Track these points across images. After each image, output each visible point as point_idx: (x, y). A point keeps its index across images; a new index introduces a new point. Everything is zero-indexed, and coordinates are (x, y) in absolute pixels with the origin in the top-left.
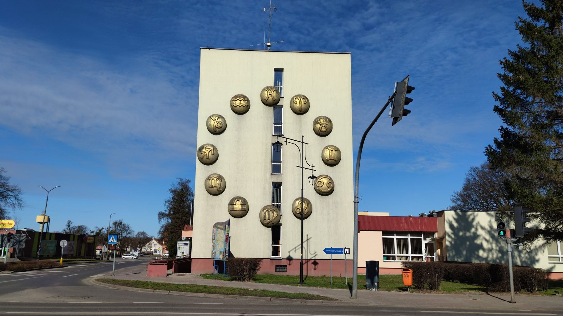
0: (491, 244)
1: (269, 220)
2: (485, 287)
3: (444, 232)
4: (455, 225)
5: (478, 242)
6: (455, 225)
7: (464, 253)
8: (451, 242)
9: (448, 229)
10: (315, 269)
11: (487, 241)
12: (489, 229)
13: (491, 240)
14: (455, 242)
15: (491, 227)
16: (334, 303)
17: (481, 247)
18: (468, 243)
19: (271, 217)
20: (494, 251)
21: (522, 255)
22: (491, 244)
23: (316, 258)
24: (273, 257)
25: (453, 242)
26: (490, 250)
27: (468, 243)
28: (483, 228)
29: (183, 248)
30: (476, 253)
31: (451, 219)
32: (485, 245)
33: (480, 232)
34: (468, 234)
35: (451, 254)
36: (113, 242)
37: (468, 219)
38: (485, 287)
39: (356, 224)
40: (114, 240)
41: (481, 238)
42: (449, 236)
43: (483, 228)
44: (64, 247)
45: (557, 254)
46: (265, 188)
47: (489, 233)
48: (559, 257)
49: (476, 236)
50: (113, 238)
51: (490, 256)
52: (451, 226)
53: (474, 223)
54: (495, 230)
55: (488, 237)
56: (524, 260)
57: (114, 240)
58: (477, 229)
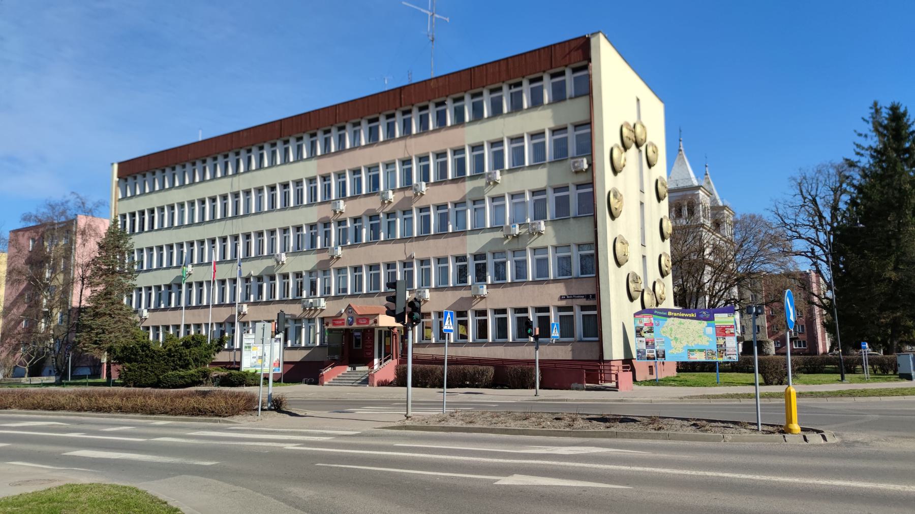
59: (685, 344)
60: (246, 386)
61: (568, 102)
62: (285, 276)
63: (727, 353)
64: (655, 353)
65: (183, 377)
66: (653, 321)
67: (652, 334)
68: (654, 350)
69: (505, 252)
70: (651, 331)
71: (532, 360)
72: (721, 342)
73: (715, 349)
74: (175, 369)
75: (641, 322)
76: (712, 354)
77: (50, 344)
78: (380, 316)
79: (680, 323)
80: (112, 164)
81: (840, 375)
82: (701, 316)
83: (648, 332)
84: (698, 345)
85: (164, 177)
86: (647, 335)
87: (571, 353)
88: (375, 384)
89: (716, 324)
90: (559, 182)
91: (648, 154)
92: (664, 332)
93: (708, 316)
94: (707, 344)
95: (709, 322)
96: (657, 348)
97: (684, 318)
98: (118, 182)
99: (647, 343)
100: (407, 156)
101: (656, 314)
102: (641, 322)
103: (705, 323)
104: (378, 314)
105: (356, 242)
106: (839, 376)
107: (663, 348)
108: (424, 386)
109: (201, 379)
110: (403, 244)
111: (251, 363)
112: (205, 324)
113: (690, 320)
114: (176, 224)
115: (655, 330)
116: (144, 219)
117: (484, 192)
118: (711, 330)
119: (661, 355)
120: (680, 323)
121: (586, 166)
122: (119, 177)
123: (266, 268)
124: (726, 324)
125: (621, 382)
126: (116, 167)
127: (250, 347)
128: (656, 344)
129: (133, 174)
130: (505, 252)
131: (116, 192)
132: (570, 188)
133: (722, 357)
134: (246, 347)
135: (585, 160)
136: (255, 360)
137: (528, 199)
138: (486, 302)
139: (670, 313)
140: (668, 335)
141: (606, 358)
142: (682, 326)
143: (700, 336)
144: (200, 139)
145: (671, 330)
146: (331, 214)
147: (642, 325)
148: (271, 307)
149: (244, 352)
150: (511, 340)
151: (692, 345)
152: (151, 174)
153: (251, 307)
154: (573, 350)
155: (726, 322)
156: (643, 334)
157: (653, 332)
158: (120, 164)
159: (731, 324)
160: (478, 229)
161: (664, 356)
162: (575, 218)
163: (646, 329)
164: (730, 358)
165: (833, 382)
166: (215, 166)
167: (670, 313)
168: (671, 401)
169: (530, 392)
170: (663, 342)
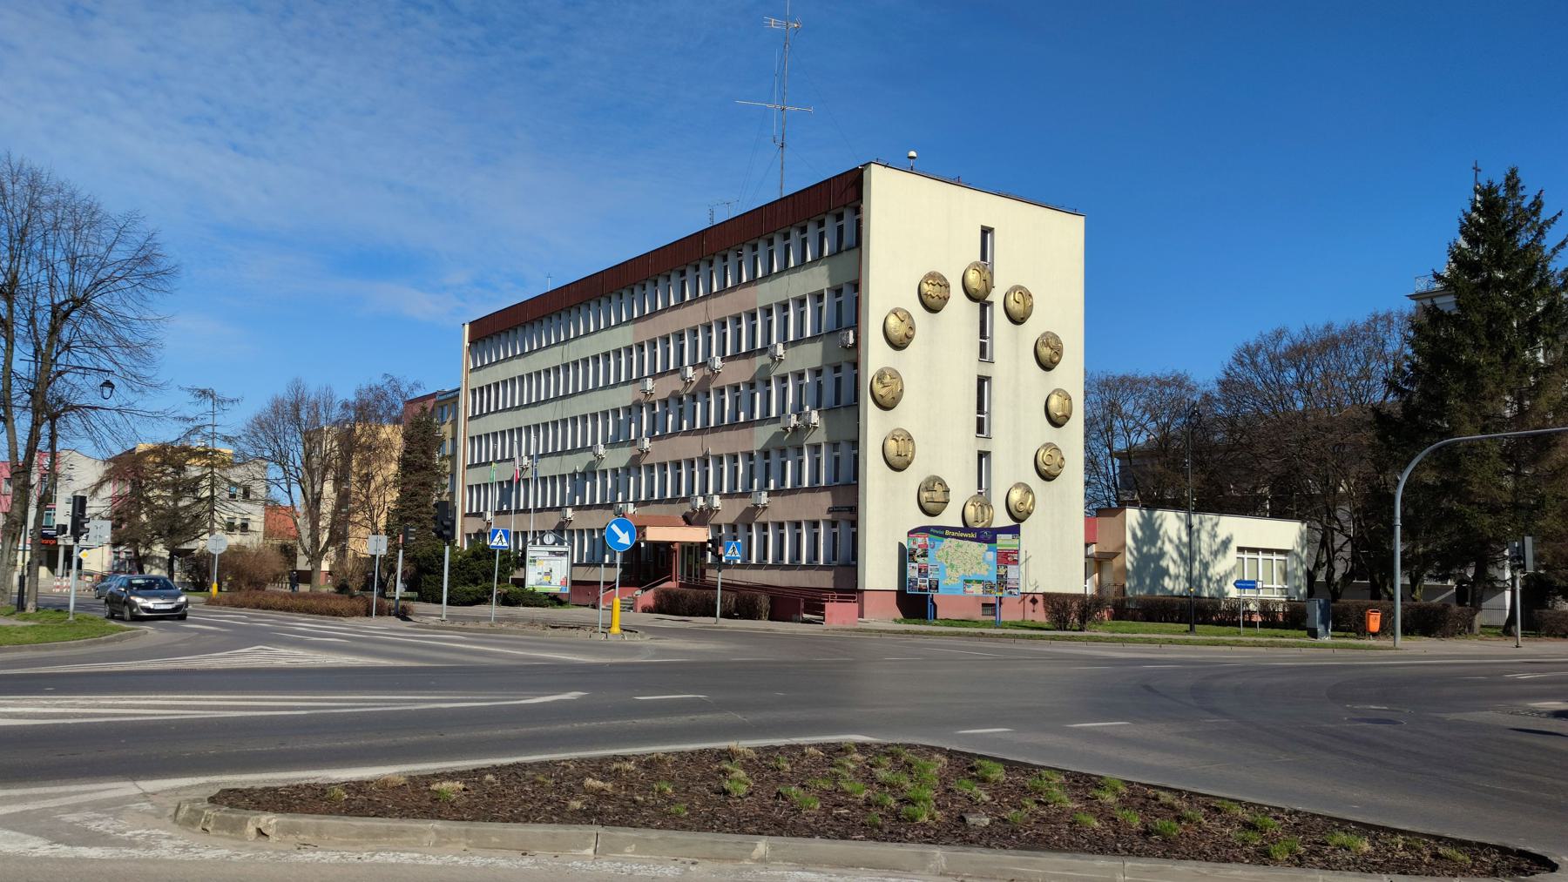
0: (1179, 567)
1: (31, 371)
2: (1378, 581)
3: (1119, 543)
4: (1139, 534)
5: (1164, 563)
6: (1139, 534)
7: (1148, 581)
8: (1132, 564)
9: (1130, 542)
10: (1034, 611)
11: (1174, 562)
12: (1176, 541)
13: (1179, 560)
14: (1138, 564)
15: (1180, 539)
16: (739, 781)
17: (1166, 572)
18: (1152, 566)
19: (986, 517)
20: (1181, 579)
21: (1211, 586)
22: (1179, 567)
23: (1037, 592)
24: (409, 594)
25: (1135, 564)
26: (1177, 577)
27: (1152, 566)
28: (1171, 541)
29: (545, 562)
30: (1161, 582)
31: (1135, 524)
32: (1173, 570)
33: (1168, 547)
34: (1153, 551)
35: (1132, 585)
36: (500, 544)
37: (1154, 524)
38: (1378, 581)
39: (860, 496)
40: (737, 552)
41: (1168, 556)
42: (1131, 553)
43: (1171, 541)
44: (219, 555)
45: (589, 589)
46: (968, 462)
47: (1177, 548)
48: (1273, 589)
49: (1162, 554)
50: (501, 536)
51: (1177, 587)
52: (1134, 536)
53: (1161, 533)
54: (1184, 545)
55: (1175, 556)
56: (1212, 592)
57: (737, 552)
58: (1163, 543)
59: (962, 572)
60: (524, 606)
61: (845, 253)
62: (604, 473)
63: (1008, 586)
64: (927, 584)
65: (468, 593)
66: (928, 543)
67: (926, 559)
68: (927, 579)
69: (785, 450)
70: (924, 555)
71: (626, 586)
72: (1002, 571)
73: (994, 580)
74: (465, 584)
75: (914, 543)
76: (991, 587)
77: (1450, 501)
78: (648, 528)
79: (958, 546)
80: (464, 325)
81: (1189, 625)
82: (982, 537)
83: (922, 556)
84: (975, 574)
85: (711, 273)
86: (920, 560)
87: (832, 581)
88: (639, 609)
89: (998, 548)
90: (834, 360)
91: (887, 326)
92: (939, 557)
93: (990, 537)
94: (986, 573)
95: (991, 545)
96: (931, 577)
97: (963, 538)
98: (470, 347)
99: (920, 570)
100: (708, 321)
101: (932, 533)
102: (914, 543)
103: (986, 545)
104: (645, 527)
105: (836, 404)
106: (1187, 627)
107: (937, 577)
108: (454, 605)
109: (485, 596)
110: (700, 437)
111: (537, 580)
112: (588, 530)
113: (969, 542)
114: (500, 408)
115: (929, 554)
116: (710, 338)
117: (769, 371)
118: (991, 556)
119: (933, 586)
120: (958, 546)
121: (851, 341)
122: (470, 342)
123: (774, 435)
124: (1010, 548)
125: (830, 615)
126: (467, 327)
127: (535, 561)
128: (929, 572)
129: (597, 297)
130: (785, 450)
131: (467, 362)
132: (843, 368)
133: (1001, 591)
134: (531, 561)
135: (851, 333)
136: (540, 576)
137: (808, 381)
138: (767, 513)
139: (947, 533)
140: (943, 560)
141: (860, 587)
142: (960, 549)
143: (979, 563)
144: (549, 290)
145: (948, 554)
146: (679, 386)
147: (915, 547)
148: (675, 506)
149: (529, 567)
150: (822, 563)
151: (971, 575)
152: (641, 288)
153: (725, 501)
154: (835, 578)
155: (1010, 546)
156: (918, 559)
157: (927, 556)
158: (470, 323)
159: (1015, 548)
160: (766, 419)
161: (937, 588)
162: (844, 407)
163: (919, 551)
164: (1011, 593)
165: (1179, 633)
166: (755, 259)
167: (947, 533)
168: (704, 627)
169: (713, 619)
170: (938, 570)
